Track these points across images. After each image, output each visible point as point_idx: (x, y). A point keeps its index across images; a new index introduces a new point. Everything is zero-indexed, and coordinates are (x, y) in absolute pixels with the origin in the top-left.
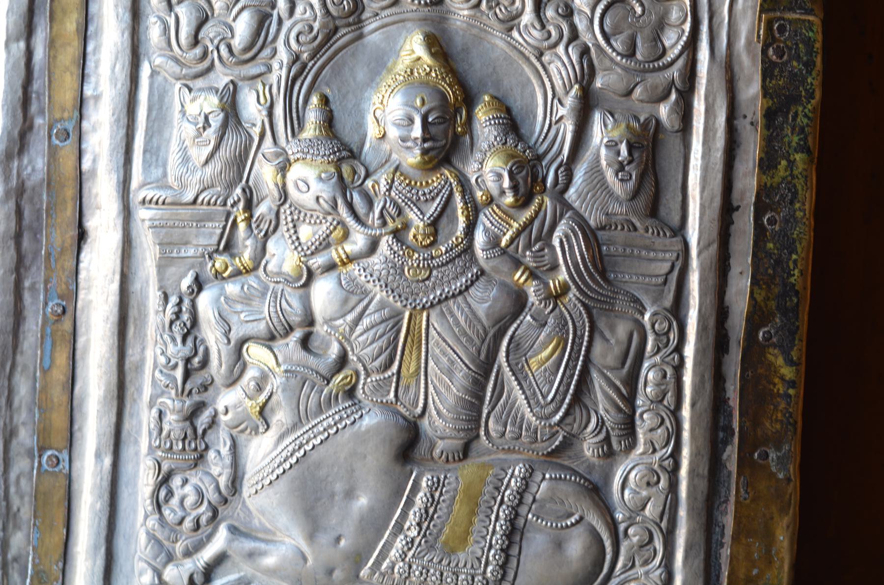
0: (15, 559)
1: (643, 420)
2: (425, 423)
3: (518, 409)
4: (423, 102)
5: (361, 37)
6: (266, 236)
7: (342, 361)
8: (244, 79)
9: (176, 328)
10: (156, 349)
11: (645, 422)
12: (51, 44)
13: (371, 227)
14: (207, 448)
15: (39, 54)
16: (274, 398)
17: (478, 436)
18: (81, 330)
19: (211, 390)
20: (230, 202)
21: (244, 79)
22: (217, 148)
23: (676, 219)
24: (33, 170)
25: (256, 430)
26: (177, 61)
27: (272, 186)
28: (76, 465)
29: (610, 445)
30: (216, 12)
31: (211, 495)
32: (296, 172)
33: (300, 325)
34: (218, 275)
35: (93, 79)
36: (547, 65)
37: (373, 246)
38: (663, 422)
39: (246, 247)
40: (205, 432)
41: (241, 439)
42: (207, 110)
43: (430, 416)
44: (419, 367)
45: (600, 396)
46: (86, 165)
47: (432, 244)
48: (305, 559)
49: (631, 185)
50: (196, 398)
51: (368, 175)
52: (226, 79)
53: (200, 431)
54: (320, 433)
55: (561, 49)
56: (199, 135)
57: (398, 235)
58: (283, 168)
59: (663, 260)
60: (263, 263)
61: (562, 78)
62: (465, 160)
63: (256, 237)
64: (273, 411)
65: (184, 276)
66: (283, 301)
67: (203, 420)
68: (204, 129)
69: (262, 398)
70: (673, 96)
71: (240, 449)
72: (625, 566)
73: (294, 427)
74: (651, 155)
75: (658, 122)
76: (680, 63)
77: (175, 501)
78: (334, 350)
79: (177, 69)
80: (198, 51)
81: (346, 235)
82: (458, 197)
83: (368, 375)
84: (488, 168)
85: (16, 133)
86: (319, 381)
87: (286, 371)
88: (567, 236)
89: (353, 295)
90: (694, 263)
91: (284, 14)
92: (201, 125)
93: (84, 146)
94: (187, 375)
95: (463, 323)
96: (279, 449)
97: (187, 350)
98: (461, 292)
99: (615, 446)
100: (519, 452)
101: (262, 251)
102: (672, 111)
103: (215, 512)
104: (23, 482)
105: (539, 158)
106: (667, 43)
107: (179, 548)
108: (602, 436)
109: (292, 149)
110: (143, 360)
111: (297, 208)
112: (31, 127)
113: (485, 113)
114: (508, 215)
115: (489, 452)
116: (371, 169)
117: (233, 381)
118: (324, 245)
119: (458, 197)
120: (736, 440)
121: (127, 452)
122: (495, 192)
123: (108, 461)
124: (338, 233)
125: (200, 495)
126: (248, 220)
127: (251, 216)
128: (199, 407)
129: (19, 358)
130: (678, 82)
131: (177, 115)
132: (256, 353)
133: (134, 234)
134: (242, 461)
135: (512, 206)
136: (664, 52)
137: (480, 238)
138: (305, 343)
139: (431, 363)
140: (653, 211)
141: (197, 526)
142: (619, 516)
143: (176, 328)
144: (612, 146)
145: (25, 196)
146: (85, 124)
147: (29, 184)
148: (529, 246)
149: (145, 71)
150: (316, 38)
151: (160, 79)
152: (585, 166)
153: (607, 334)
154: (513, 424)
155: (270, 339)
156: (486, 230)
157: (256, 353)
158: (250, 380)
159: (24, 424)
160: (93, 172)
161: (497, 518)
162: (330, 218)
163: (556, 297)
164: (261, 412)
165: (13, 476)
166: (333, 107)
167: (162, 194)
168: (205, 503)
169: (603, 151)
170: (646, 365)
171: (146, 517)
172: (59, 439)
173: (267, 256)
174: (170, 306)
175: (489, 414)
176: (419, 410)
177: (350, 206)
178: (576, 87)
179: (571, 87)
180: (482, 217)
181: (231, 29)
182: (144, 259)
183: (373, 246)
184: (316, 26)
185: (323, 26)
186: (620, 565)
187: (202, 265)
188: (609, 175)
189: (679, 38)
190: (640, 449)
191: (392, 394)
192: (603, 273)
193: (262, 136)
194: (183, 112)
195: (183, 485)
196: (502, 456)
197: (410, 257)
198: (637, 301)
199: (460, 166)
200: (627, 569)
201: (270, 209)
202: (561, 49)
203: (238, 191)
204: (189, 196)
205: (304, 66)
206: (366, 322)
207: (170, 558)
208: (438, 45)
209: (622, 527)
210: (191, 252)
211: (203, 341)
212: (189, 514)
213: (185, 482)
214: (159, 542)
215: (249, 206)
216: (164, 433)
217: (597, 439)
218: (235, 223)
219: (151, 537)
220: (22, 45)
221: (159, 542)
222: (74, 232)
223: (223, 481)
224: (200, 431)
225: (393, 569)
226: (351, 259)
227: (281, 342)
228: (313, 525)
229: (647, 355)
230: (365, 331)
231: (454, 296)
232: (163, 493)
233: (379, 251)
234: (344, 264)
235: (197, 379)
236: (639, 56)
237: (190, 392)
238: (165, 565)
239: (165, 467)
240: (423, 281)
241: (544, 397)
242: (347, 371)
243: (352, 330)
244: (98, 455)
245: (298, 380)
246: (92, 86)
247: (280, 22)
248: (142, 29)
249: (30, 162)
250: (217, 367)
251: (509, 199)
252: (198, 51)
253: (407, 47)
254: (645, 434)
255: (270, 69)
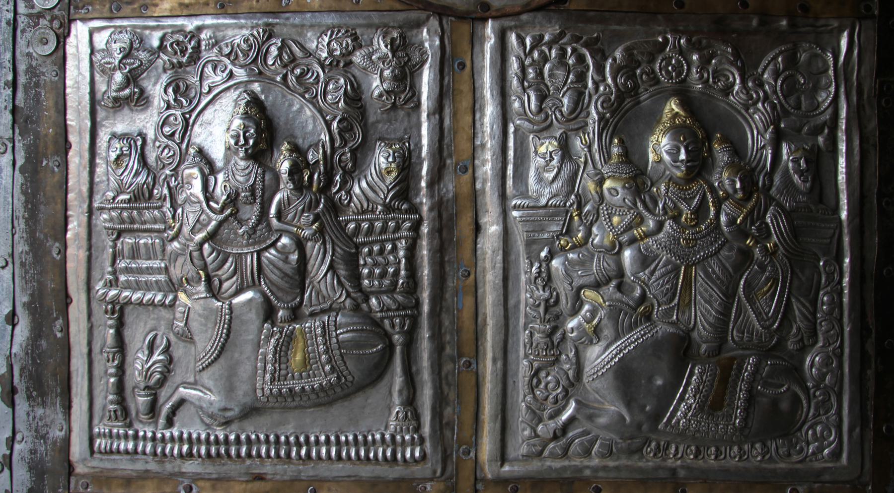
0: (448, 424)
1: (822, 326)
2: (695, 335)
3: (754, 326)
4: (684, 138)
5: (639, 103)
6: (592, 224)
7: (643, 297)
8: (572, 130)
9: (539, 281)
10: (526, 295)
11: (823, 327)
12: (454, 115)
13: (658, 215)
14: (561, 354)
15: (447, 122)
16: (603, 322)
17: (727, 340)
18: (480, 285)
19: (561, 318)
20: (568, 204)
21: (572, 130)
22: (558, 173)
23: (833, 203)
24: (447, 191)
25: (591, 342)
26: (530, 121)
27: (593, 192)
28: (481, 366)
29: (803, 343)
30: (551, 92)
31: (563, 382)
32: (608, 184)
33: (616, 277)
34: (563, 249)
35: (480, 135)
36: (95, 211)
37: (660, 226)
38: (834, 327)
39: (579, 231)
40: (559, 343)
41: (581, 347)
42: (551, 149)
43: (698, 329)
44: (691, 300)
45: (797, 312)
46: (478, 186)
47: (697, 225)
48: (625, 419)
49: (808, 185)
50: (553, 324)
51: (652, 185)
52: (561, 131)
53: (556, 343)
54: (633, 342)
55: (760, 105)
56: (547, 165)
57: (676, 219)
58: (600, 183)
59: (829, 228)
60: (591, 240)
61: (762, 122)
62: (711, 174)
63: (585, 224)
64: (601, 330)
65: (542, 250)
66: (605, 264)
67: (558, 336)
68: (551, 161)
69: (595, 322)
70: (826, 131)
71: (581, 353)
72: (814, 414)
73: (617, 338)
74: (819, 164)
75: (818, 146)
76: (830, 111)
77: (542, 386)
78: (638, 292)
79: (530, 126)
80: (543, 115)
81: (642, 221)
82: (709, 196)
83: (659, 306)
84: (724, 178)
85: (436, 169)
86: (629, 311)
87: (609, 306)
88: (774, 215)
89: (644, 261)
90: (846, 231)
91: (592, 92)
92: (548, 159)
93: (476, 175)
94: (546, 310)
95: (717, 271)
96: (607, 353)
97: (547, 294)
98: (715, 254)
99: (806, 343)
100: (751, 349)
101: (589, 233)
102: (826, 140)
103: (566, 390)
104: (450, 377)
105: (753, 170)
106: (820, 99)
107: (546, 414)
108: (800, 337)
109: (605, 170)
110: (519, 302)
111: (610, 206)
112: (445, 165)
113: (719, 145)
114: (740, 204)
115: (733, 350)
116: (655, 179)
117: (575, 312)
118: (629, 228)
119: (709, 196)
120: (873, 335)
121: (511, 357)
122: (730, 191)
123: (499, 364)
124: (638, 220)
125: (558, 383)
126: (579, 215)
127: (581, 213)
128: (555, 329)
129: (444, 304)
130: (828, 123)
131: (532, 154)
132: (588, 294)
133: (509, 226)
134: (582, 360)
135: (740, 200)
136: (818, 106)
137: (723, 218)
138: (619, 287)
139: (699, 297)
140: (821, 200)
141: (556, 401)
142: (810, 384)
143: (539, 281)
144: (796, 161)
145: (443, 207)
146: (477, 162)
147: (445, 199)
148: (752, 224)
149: (511, 129)
150: (613, 104)
151: (520, 132)
152: (780, 173)
153: (800, 275)
154: (748, 333)
155: (597, 286)
156: (727, 214)
157: (588, 294)
158: (587, 312)
159: (449, 343)
160: (483, 191)
161: (741, 390)
162: (632, 211)
163: (771, 254)
164: (595, 331)
165: (443, 374)
166: (626, 145)
167: (525, 202)
168: (561, 387)
169: (790, 165)
170: (821, 293)
171: (525, 396)
172: (469, 349)
173: (593, 236)
174: (534, 268)
175: (733, 328)
176: (691, 325)
177: (644, 203)
178: (772, 127)
179: (769, 127)
180: (723, 206)
181: (561, 101)
182: (516, 241)
183: (660, 226)
184: (613, 97)
185: (617, 97)
186: (811, 414)
187: (553, 242)
188: (796, 178)
189: (828, 96)
190: (820, 344)
191: (675, 317)
192: (796, 237)
193: (586, 163)
194: (536, 152)
195: (547, 376)
196: (741, 352)
197: (684, 233)
198: (815, 254)
199: (707, 177)
200: (814, 416)
201: (594, 208)
202: (760, 105)
203: (573, 197)
204: (543, 201)
205: (608, 121)
206: (658, 273)
207: (540, 420)
208: (686, 102)
209: (812, 391)
210: (546, 236)
211: (555, 289)
212: (550, 394)
213: (548, 375)
214: (534, 412)
215: (580, 207)
216: (534, 345)
217: (797, 339)
218: (572, 217)
219: (528, 408)
220: (437, 116)
221: (534, 412)
222: (473, 227)
223: (571, 373)
224: (556, 343)
225: (679, 423)
226: (647, 235)
227: (604, 288)
228: (629, 401)
229: (822, 286)
230: (657, 280)
231: (711, 256)
232: (535, 381)
233: (664, 229)
234: (642, 239)
235: (555, 310)
236: (803, 108)
237: (549, 320)
238: (537, 425)
239: (536, 364)
240: (692, 247)
241: (767, 314)
242: (647, 304)
243: (649, 279)
244: (494, 360)
245: (615, 313)
246: (480, 139)
247: (590, 96)
248: (508, 103)
249: (444, 186)
250: (565, 304)
251: (740, 195)
252: (543, 115)
253: (668, 107)
254: (823, 334)
255: (587, 125)
